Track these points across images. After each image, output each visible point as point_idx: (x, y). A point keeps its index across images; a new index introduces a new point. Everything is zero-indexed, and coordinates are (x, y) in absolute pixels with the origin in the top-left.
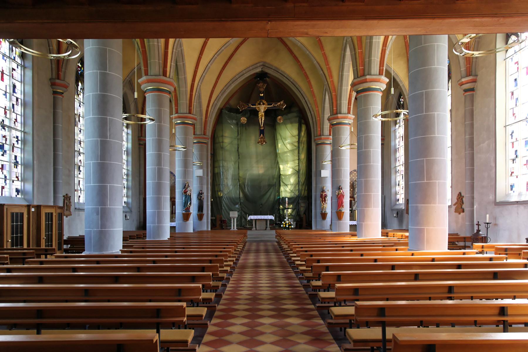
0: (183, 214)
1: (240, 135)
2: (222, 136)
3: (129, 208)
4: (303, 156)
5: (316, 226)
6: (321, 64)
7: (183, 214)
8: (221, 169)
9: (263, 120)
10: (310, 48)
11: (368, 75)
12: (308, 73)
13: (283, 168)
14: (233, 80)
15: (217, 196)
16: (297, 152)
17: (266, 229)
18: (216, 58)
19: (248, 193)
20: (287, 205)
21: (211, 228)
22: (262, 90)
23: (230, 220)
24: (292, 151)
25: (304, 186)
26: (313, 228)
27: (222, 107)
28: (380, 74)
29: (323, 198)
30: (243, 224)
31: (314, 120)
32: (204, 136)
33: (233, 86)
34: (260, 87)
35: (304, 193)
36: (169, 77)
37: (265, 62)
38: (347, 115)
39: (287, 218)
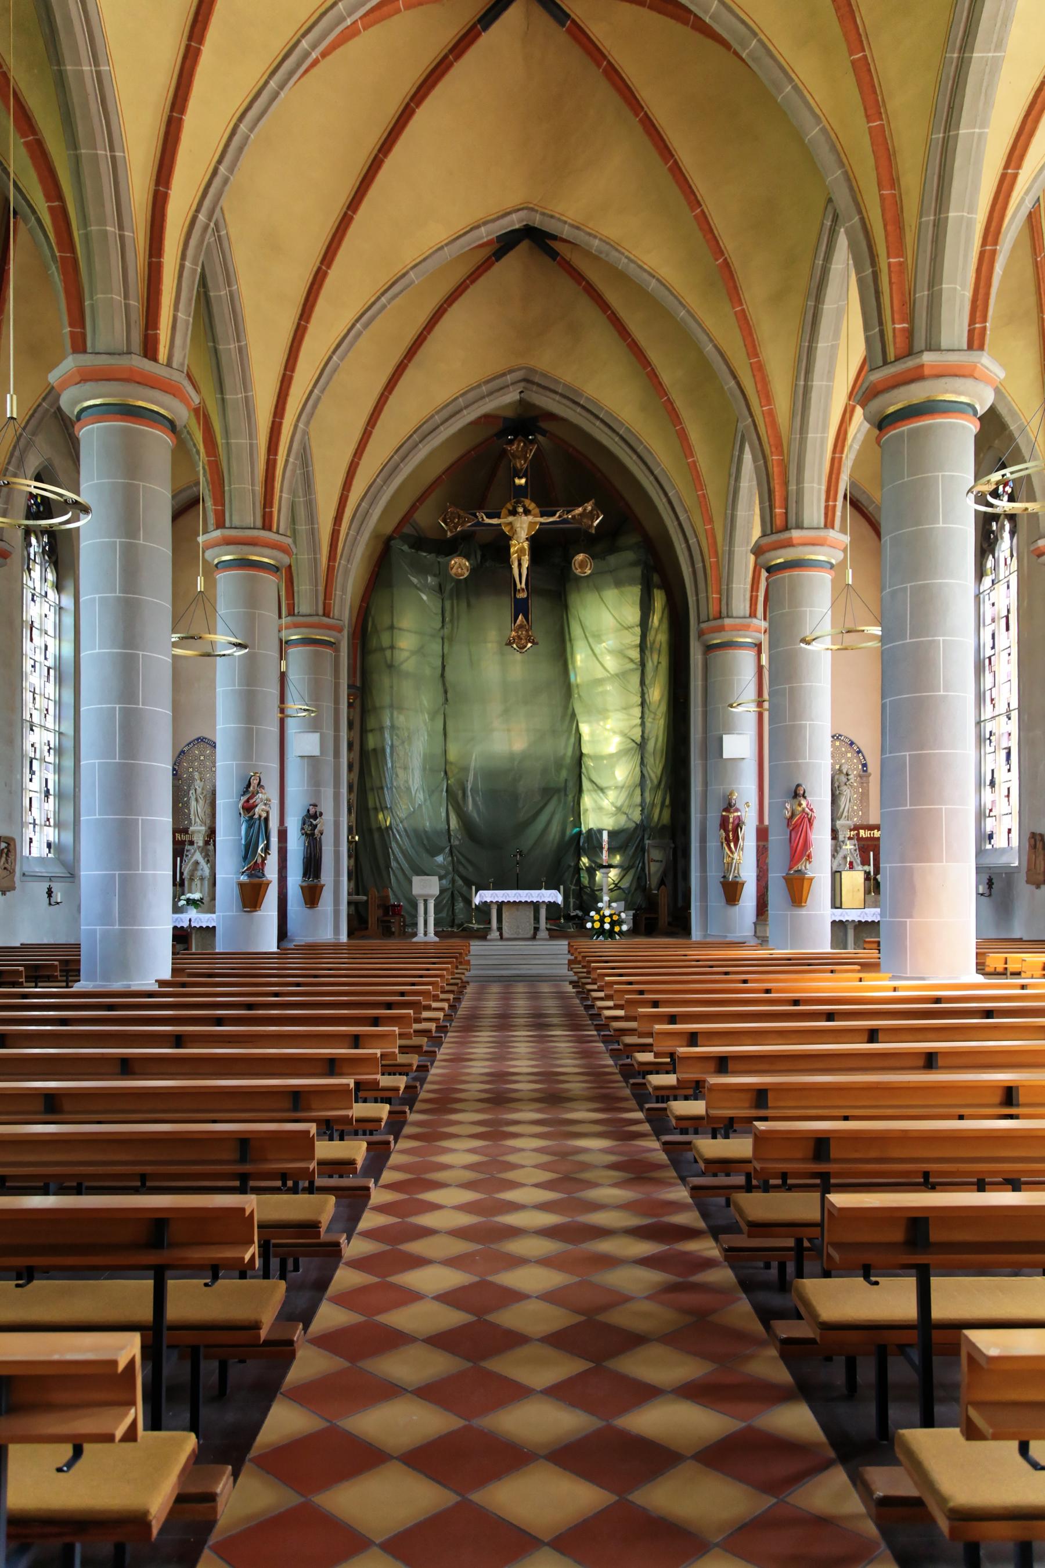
0: (241, 885)
1: (448, 626)
2: (392, 627)
3: (63, 863)
4: (657, 694)
5: (705, 927)
6: (729, 354)
7: (241, 885)
8: (387, 735)
9: (525, 564)
10: (692, 300)
11: (929, 349)
12: (679, 404)
13: (592, 734)
14: (423, 432)
15: (374, 826)
16: (636, 679)
17: (534, 937)
18: (359, 334)
19: (475, 815)
20: (605, 854)
21: (350, 934)
22: (521, 464)
23: (415, 906)
24: (621, 676)
25: (660, 794)
26: (696, 934)
27: (389, 529)
28: (970, 347)
29: (731, 831)
30: (460, 917)
31: (699, 565)
32: (325, 620)
33: (423, 451)
34: (514, 456)
35: (661, 816)
36: (169, 365)
37: (532, 370)
38: (822, 533)
39: (606, 898)
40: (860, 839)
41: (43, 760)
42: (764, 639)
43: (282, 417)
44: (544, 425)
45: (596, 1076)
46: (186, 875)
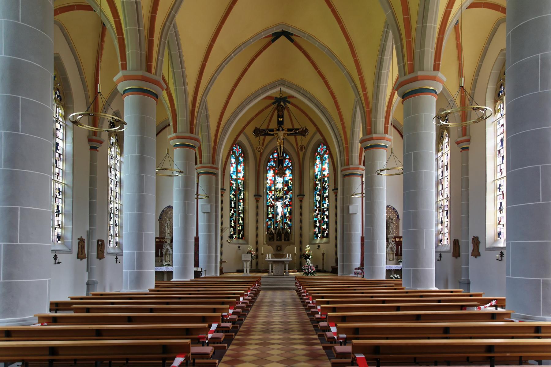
28: (434, 70)
40: (396, 241)
41: (114, 214)
42: (364, 172)
43: (197, 95)
44: (288, 99)
45: (302, 323)
46: (164, 253)
